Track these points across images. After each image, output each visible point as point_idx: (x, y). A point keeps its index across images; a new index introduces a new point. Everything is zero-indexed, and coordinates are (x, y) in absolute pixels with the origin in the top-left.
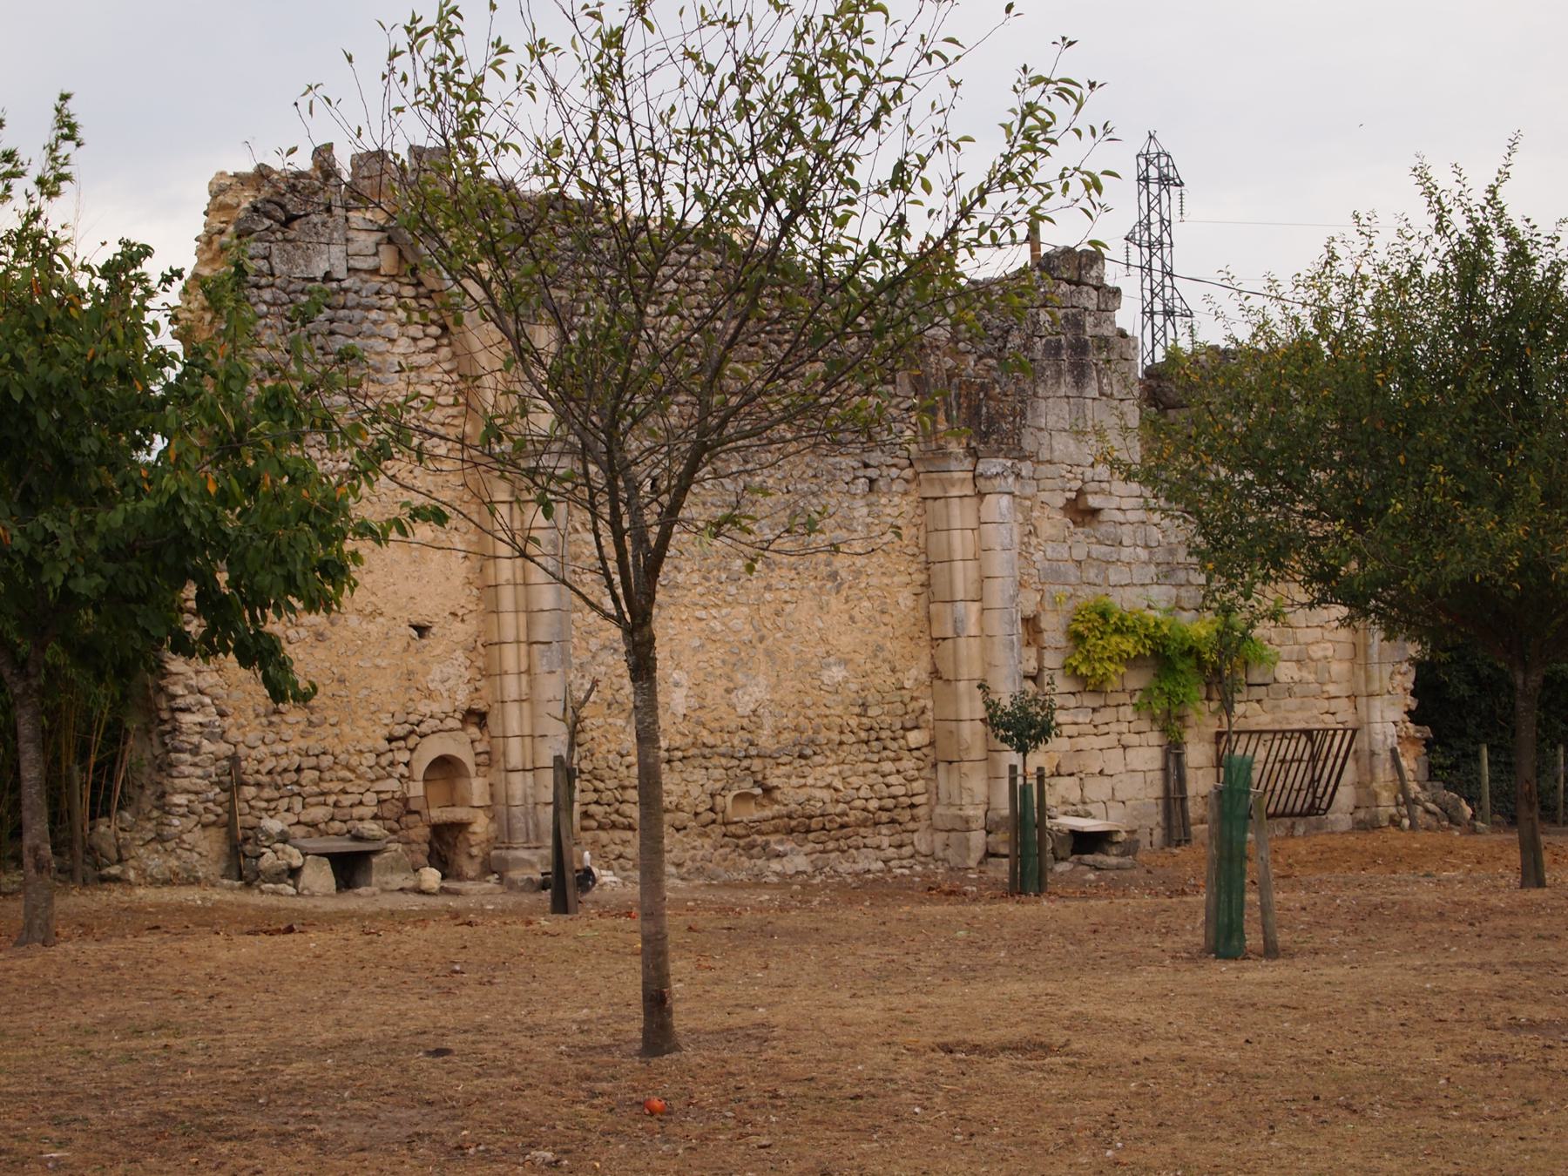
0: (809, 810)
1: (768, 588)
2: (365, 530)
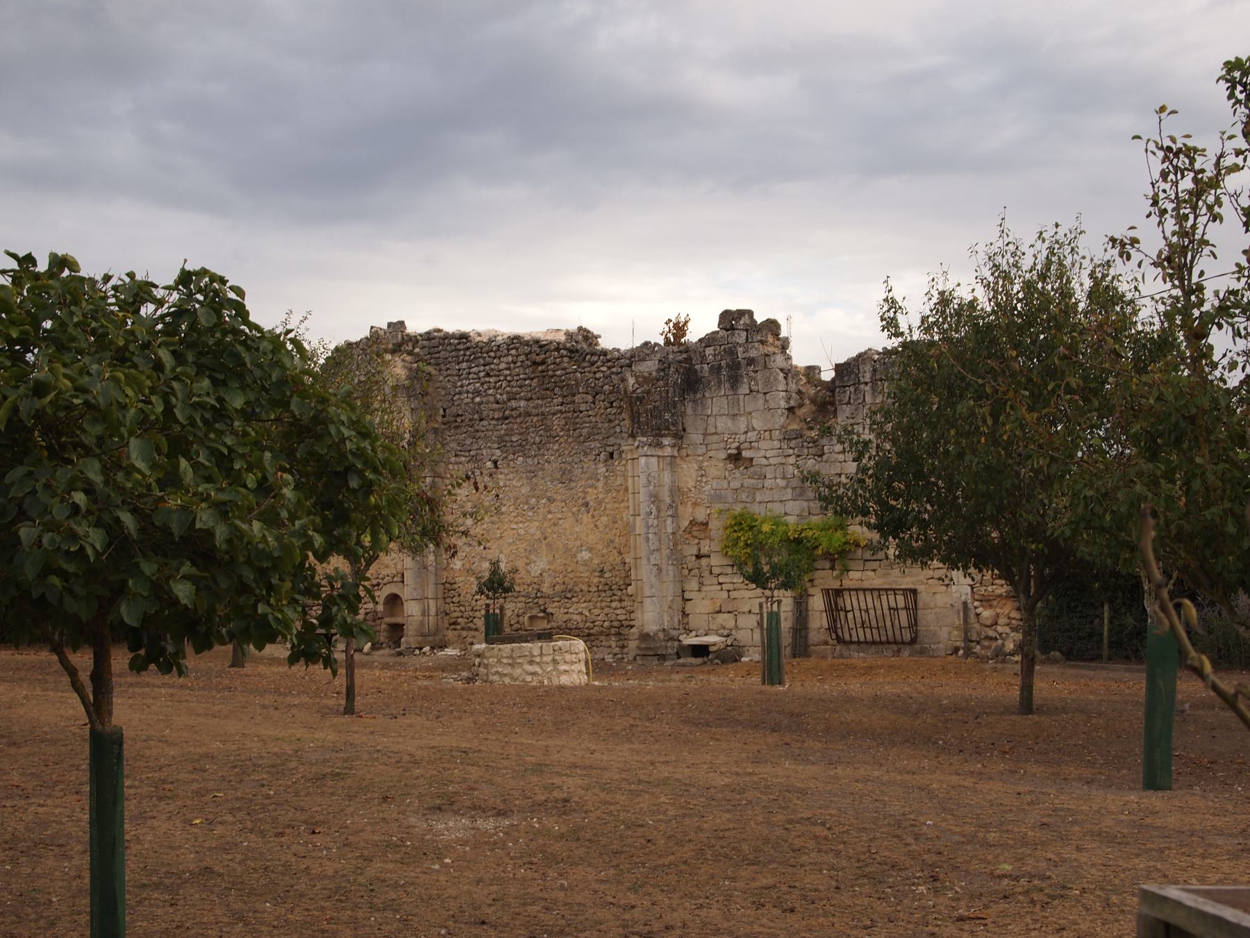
0: (569, 625)
1: (549, 512)
2: (802, 472)
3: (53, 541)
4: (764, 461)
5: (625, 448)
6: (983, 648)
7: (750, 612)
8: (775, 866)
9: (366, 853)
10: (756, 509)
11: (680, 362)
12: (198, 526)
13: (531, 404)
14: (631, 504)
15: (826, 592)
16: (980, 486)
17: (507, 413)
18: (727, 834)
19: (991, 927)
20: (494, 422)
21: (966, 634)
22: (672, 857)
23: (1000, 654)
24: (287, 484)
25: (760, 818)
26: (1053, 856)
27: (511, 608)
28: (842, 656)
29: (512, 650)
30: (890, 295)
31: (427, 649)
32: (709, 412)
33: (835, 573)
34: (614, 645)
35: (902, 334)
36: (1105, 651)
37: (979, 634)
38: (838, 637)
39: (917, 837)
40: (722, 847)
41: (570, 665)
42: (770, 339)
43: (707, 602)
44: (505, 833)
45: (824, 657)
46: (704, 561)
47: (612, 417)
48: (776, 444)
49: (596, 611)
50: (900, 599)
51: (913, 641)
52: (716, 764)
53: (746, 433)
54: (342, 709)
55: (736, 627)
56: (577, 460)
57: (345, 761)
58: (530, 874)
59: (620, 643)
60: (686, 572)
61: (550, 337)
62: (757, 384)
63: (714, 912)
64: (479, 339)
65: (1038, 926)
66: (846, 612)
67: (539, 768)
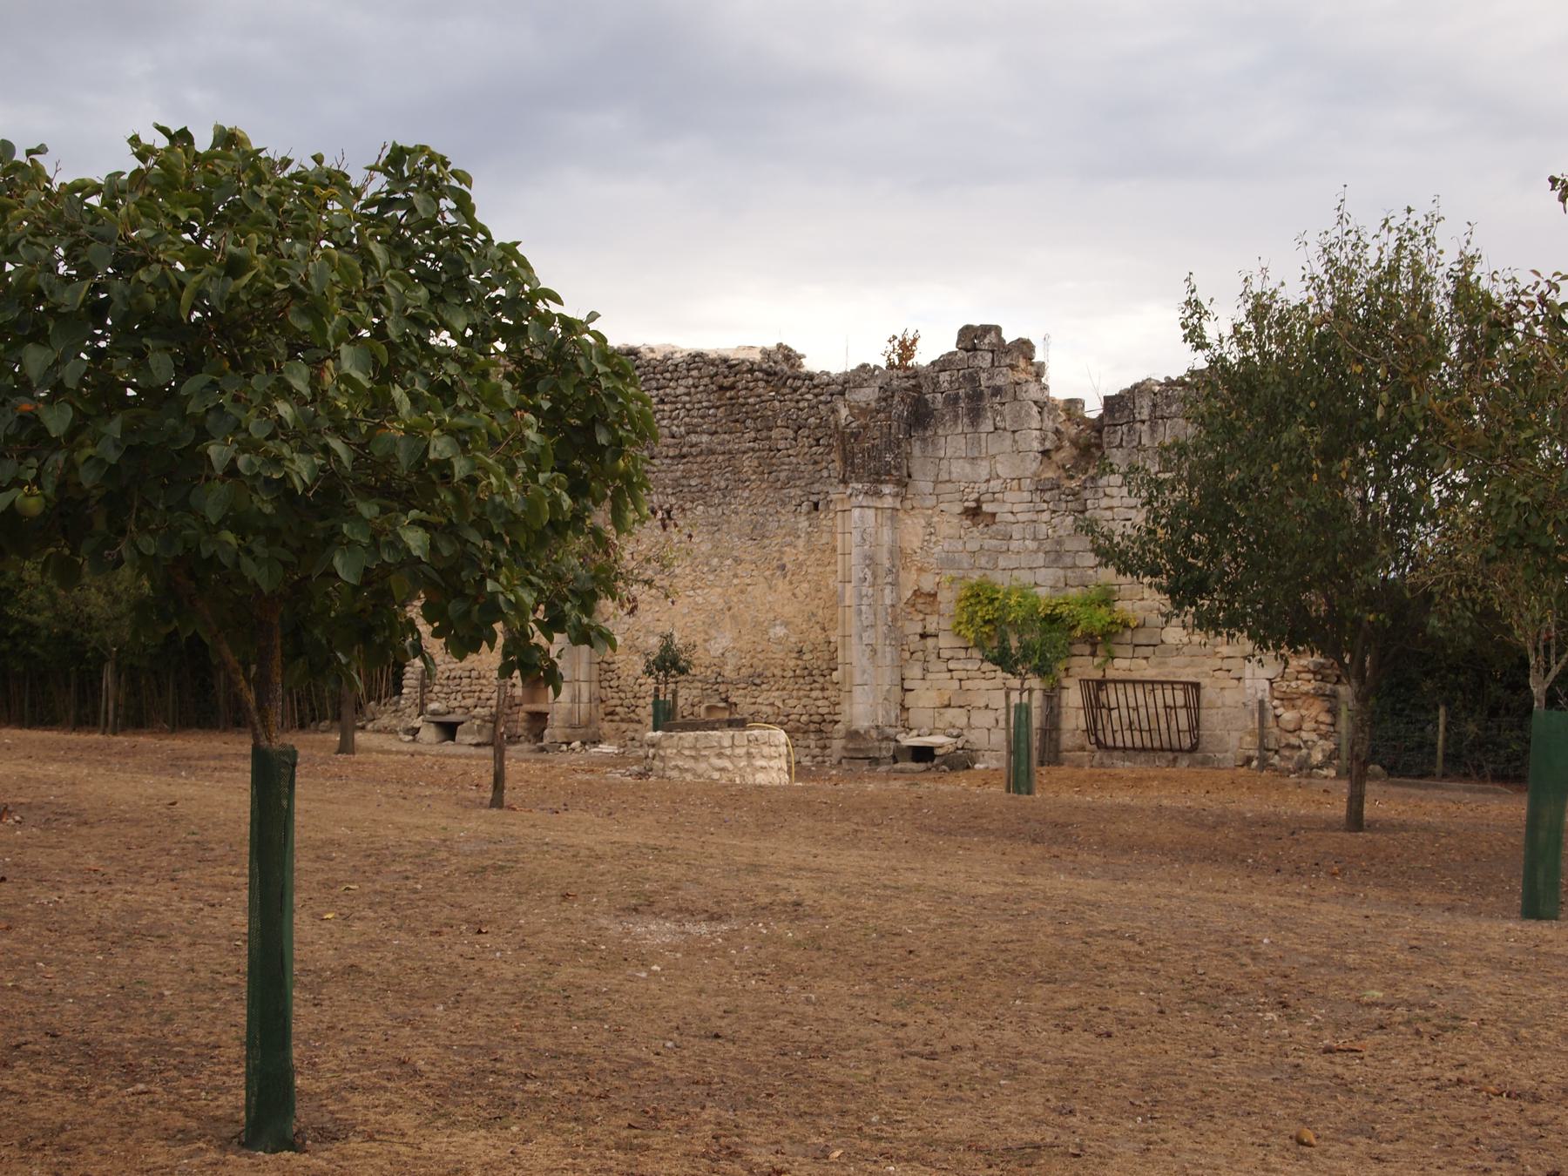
1: (736, 576)
3: (251, 464)
4: (1011, 518)
5: (833, 497)
6: (1282, 758)
7: (987, 707)
8: (1076, 984)
9: (550, 957)
10: (1001, 580)
11: (906, 389)
12: (432, 456)
13: (715, 439)
14: (839, 567)
15: (1085, 683)
16: (1307, 537)
17: (685, 450)
18: (1010, 946)
19: (1368, 1060)
20: (668, 461)
21: (1261, 740)
22: (943, 972)
23: (1305, 768)
24: (530, 426)
25: (1050, 930)
26: (1435, 983)
27: (686, 696)
28: (1102, 765)
29: (697, 739)
30: (1194, 296)
31: (576, 744)
32: (942, 454)
33: (1097, 661)
34: (813, 745)
35: (1208, 345)
36: (1439, 767)
37: (1278, 741)
38: (1098, 741)
39: (1255, 957)
40: (1006, 961)
41: (767, 759)
42: (1022, 363)
43: (933, 694)
44: (725, 939)
45: (1080, 766)
46: (930, 642)
47: (818, 458)
48: (1026, 496)
49: (792, 702)
50: (1180, 695)
51: (1194, 748)
52: (980, 873)
53: (988, 481)
54: (487, 802)
55: (969, 726)
56: (772, 511)
57: (508, 852)
58: (763, 987)
59: (821, 743)
60: (907, 655)
61: (742, 355)
62: (1004, 420)
63: (1009, 1033)
64: (651, 355)
65: (1430, 1061)
66: (1110, 709)
67: (755, 869)
